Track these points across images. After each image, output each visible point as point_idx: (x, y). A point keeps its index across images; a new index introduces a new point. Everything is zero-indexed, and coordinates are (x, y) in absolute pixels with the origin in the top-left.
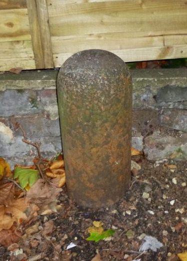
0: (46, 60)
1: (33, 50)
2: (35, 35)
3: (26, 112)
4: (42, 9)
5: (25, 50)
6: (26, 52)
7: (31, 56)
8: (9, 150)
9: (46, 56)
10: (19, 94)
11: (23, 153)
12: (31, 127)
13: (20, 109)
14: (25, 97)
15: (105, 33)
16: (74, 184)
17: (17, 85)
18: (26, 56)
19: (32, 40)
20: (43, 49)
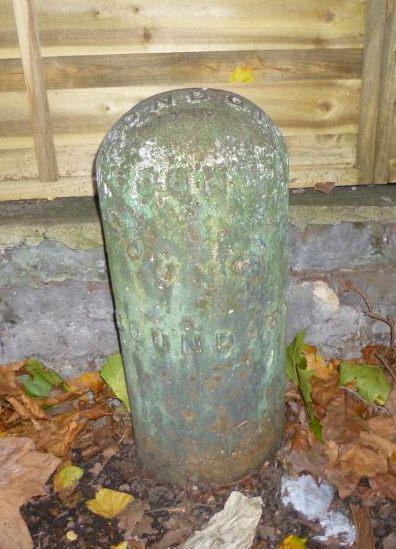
0: (378, 169)
1: (358, 152)
2: (369, 125)
3: (362, 263)
4: (390, 83)
5: (339, 151)
6: (340, 154)
7: (348, 160)
8: (321, 332)
9: (379, 164)
10: (357, 230)
11: (344, 336)
12: (370, 290)
13: (353, 258)
14: (366, 234)
15: (275, 100)
16: (346, 414)
17: (360, 214)
18: (340, 161)
19: (359, 136)
20: (377, 150)
